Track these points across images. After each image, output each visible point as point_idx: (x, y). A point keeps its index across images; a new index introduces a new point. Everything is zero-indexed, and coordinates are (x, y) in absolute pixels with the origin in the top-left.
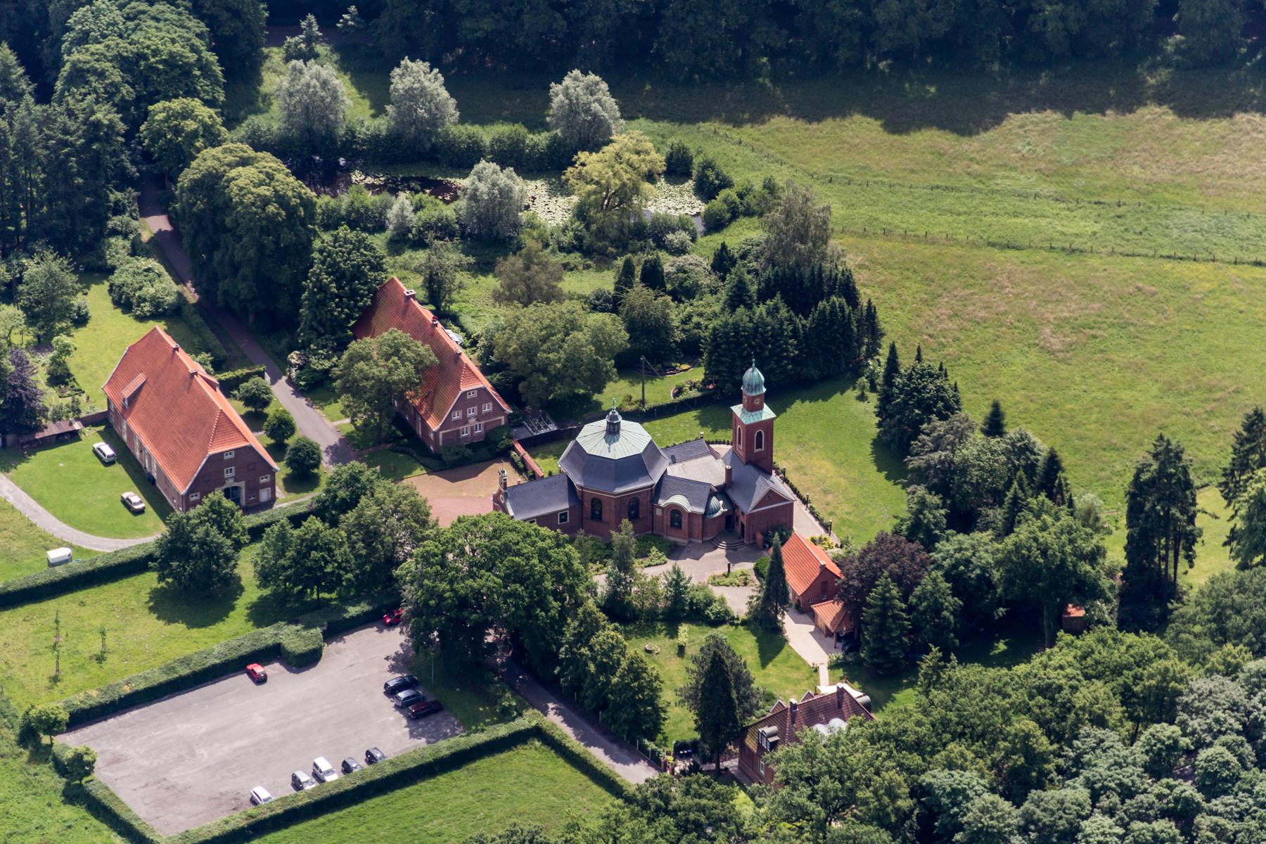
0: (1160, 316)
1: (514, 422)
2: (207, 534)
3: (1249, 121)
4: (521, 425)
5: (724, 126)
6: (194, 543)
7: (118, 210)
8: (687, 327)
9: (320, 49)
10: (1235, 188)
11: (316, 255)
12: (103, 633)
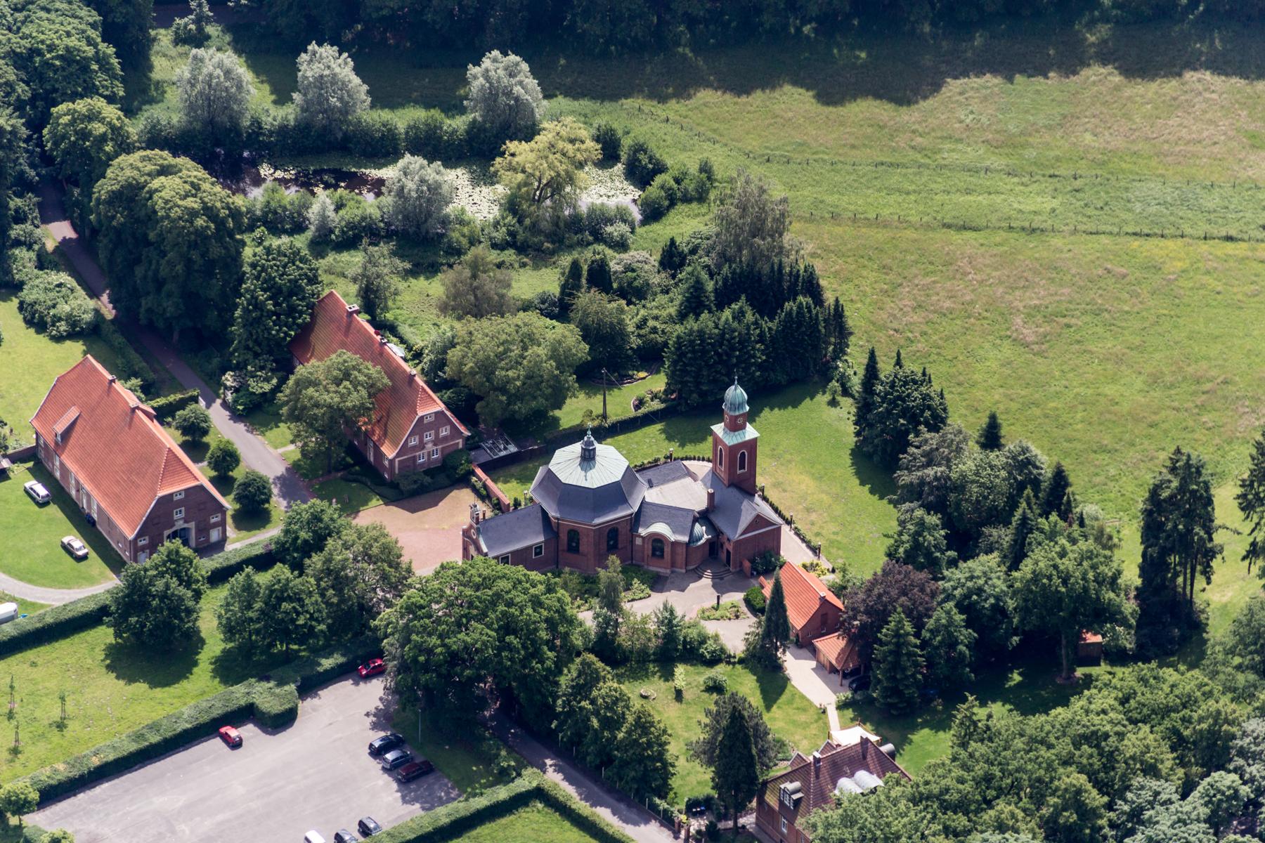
0: (1134, 300)
1: (472, 445)
2: (167, 586)
3: (1199, 80)
4: (479, 447)
5: (648, 102)
6: (154, 597)
7: (20, 218)
8: (642, 332)
9: (212, 30)
10: (1194, 155)
11: (247, 269)
12: (63, 699)
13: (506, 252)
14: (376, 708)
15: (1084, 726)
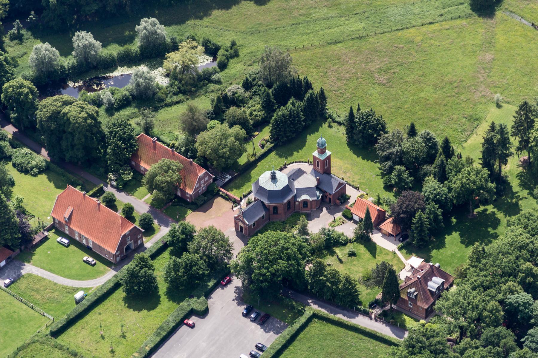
2: (145, 272)
13: (179, 95)
14: (235, 297)
15: (519, 243)
